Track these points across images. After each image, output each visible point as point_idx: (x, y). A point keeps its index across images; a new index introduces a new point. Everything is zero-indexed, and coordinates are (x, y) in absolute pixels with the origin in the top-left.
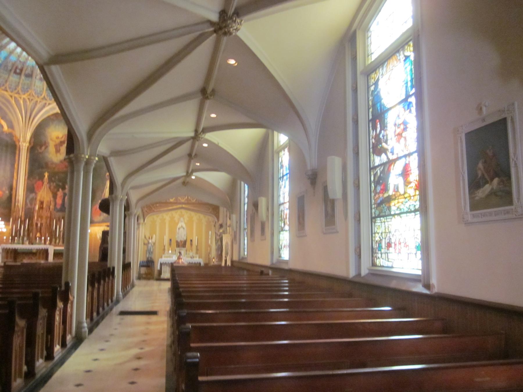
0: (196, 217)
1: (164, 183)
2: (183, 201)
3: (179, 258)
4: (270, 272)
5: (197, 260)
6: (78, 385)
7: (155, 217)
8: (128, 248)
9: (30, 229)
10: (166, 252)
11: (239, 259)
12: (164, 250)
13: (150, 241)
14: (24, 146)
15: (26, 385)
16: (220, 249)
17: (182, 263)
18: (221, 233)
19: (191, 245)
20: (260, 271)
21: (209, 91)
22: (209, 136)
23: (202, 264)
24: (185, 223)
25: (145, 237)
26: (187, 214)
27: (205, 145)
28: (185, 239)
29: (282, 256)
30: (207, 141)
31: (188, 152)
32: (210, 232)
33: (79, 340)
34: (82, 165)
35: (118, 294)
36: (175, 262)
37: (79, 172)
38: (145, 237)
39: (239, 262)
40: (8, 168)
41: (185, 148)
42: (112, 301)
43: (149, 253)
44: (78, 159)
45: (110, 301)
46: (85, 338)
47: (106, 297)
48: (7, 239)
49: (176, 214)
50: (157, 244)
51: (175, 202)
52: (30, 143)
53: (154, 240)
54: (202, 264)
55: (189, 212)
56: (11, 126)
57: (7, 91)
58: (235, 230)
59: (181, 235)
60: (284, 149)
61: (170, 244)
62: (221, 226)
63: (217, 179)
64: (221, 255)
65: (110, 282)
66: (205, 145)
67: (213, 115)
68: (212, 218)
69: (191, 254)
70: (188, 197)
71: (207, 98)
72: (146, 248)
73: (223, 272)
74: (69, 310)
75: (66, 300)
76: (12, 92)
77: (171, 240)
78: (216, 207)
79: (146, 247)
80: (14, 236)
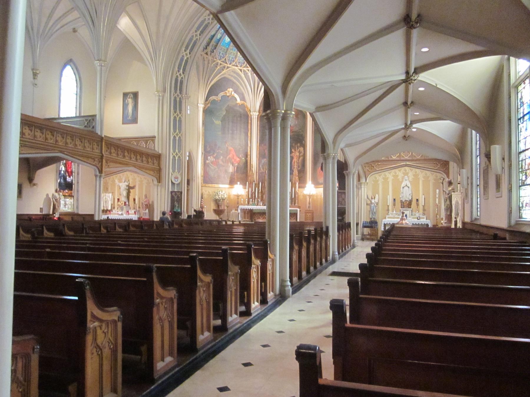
0: (421, 174)
1: (383, 137)
2: (407, 158)
3: (402, 219)
4: (507, 236)
5: (424, 221)
6: (264, 346)
7: (377, 176)
8: (348, 207)
9: (263, 191)
10: (390, 212)
11: (510, 226)
12: (388, 210)
13: (373, 201)
14: (255, 115)
15: (215, 339)
16: (449, 209)
17: (406, 223)
18: (450, 191)
19: (418, 205)
20: (493, 234)
21: (414, 16)
22: (423, 77)
23: (430, 226)
24: (410, 181)
25: (368, 198)
26: (411, 172)
27: (421, 89)
28: (410, 198)
29: (524, 216)
30: (423, 83)
31: (402, 100)
32: (438, 191)
33: (282, 298)
34: (279, 120)
35: (333, 255)
36: (397, 224)
37: (276, 127)
38: (368, 198)
39: (472, 223)
40: (243, 137)
41: (398, 94)
42: (326, 261)
43: (372, 214)
44: (274, 115)
45: (324, 260)
46: (289, 297)
47: (318, 256)
48: (244, 201)
49: (399, 173)
50: (380, 204)
51: (398, 159)
52: (259, 112)
53: (376, 200)
54: (430, 226)
55: (414, 169)
56: (243, 98)
57: (237, 66)
58: (466, 187)
59: (406, 194)
60: (523, 81)
61: (394, 205)
62: (450, 183)
63: (443, 129)
64: (451, 215)
65: (323, 241)
66: (421, 89)
67: (425, 50)
68: (441, 175)
69: (417, 215)
70: (412, 154)
71: (412, 27)
72: (369, 209)
73: (454, 236)
74: (269, 267)
75: (264, 258)
76: (241, 66)
77: (394, 200)
78: (445, 162)
79: (368, 207)
80: (251, 198)
